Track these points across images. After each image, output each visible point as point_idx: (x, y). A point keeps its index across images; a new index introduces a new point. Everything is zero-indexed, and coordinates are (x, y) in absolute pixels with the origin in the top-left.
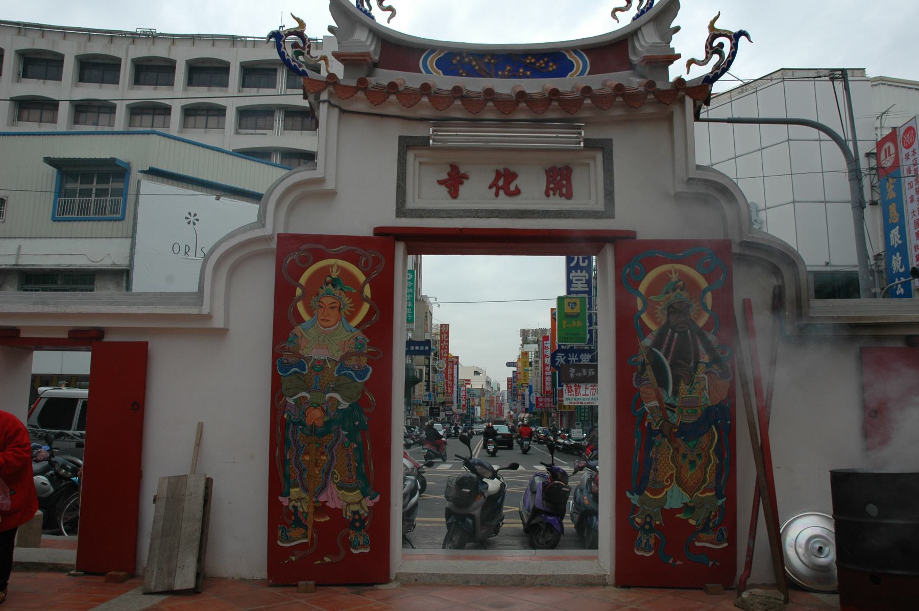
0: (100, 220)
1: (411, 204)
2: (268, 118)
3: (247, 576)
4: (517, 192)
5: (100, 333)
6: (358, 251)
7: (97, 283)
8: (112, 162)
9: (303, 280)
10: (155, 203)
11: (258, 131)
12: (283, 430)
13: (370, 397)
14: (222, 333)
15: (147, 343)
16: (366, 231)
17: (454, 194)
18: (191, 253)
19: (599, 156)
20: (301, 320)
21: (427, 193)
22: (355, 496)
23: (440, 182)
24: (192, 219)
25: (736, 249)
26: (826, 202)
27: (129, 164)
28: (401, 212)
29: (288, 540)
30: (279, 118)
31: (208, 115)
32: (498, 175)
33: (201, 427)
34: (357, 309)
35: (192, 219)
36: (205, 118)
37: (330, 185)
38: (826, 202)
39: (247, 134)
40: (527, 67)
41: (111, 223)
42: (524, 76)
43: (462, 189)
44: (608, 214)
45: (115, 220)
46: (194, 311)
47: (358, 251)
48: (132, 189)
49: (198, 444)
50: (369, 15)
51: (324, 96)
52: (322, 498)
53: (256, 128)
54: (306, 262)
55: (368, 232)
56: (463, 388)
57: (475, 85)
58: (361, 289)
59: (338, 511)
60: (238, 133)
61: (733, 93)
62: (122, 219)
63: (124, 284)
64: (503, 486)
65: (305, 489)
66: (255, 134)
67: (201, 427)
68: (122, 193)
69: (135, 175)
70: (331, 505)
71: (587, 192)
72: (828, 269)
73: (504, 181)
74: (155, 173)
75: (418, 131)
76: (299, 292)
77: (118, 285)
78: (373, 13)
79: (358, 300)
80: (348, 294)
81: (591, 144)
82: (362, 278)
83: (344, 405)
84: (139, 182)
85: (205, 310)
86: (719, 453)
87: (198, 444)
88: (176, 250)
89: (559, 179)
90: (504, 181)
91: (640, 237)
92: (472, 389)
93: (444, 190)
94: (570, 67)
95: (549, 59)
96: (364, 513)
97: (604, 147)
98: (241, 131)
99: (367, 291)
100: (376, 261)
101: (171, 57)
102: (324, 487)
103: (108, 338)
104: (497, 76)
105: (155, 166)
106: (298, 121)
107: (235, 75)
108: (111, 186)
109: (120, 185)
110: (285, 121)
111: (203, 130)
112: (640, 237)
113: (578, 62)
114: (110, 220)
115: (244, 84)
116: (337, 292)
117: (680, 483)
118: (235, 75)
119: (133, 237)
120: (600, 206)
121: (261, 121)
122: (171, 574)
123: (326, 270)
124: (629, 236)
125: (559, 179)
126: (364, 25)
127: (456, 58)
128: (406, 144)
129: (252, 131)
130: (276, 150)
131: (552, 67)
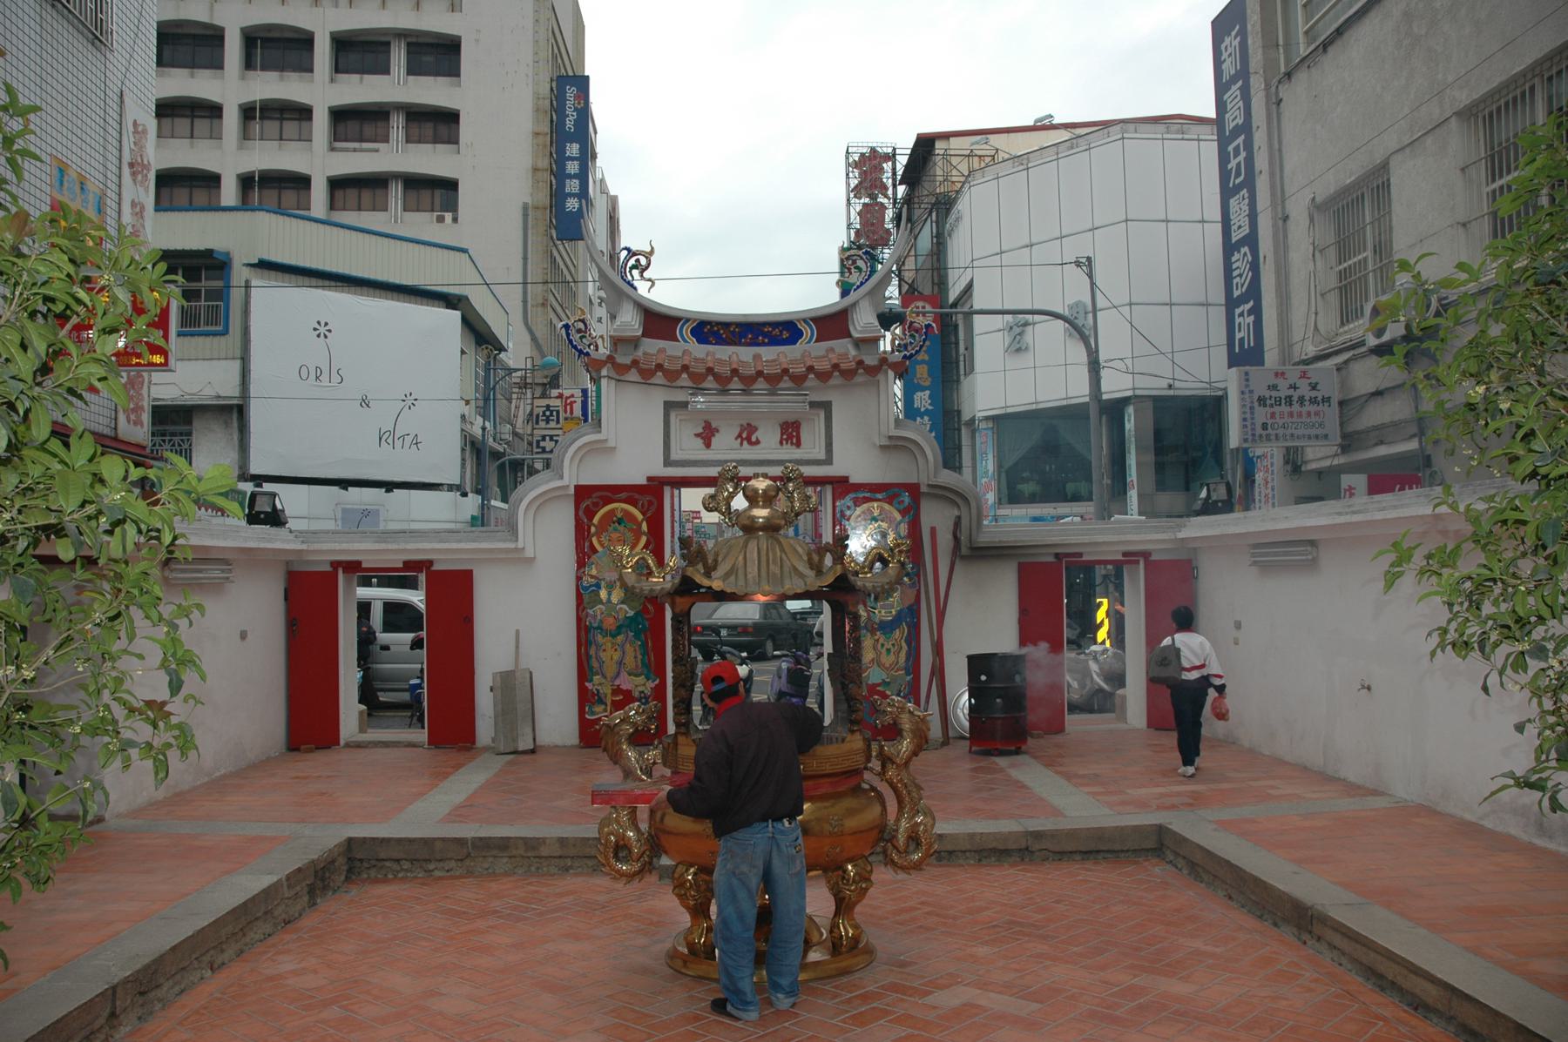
0: (192, 335)
1: (674, 456)
2: (380, 124)
3: (559, 743)
4: (758, 442)
5: (431, 562)
6: (637, 496)
7: (197, 424)
8: (209, 253)
9: (596, 521)
10: (275, 310)
11: (365, 145)
12: (585, 634)
13: (650, 607)
14: (532, 560)
15: (471, 572)
16: (640, 480)
17: (708, 445)
18: (325, 377)
19: (822, 415)
20: (595, 551)
21: (687, 445)
22: (641, 679)
23: (697, 435)
24: (322, 330)
25: (924, 489)
26: (1171, 305)
27: (228, 254)
28: (668, 462)
29: (593, 713)
30: (397, 123)
31: (282, 119)
32: (743, 429)
33: (517, 632)
34: (638, 540)
35: (322, 330)
36: (277, 123)
37: (611, 444)
38: (1171, 305)
39: (347, 150)
40: (765, 335)
41: (209, 339)
42: (763, 344)
43: (714, 440)
44: (828, 460)
45: (215, 334)
46: (512, 546)
47: (637, 496)
48: (236, 295)
49: (517, 647)
50: (632, 285)
51: (604, 372)
52: (617, 682)
53: (362, 140)
54: (598, 506)
55: (642, 481)
56: (689, 526)
57: (724, 353)
58: (640, 525)
59: (629, 692)
60: (332, 149)
61: (1062, 148)
62: (225, 333)
63: (235, 424)
64: (751, 672)
65: (604, 676)
66: (362, 150)
67: (517, 632)
68: (221, 295)
69: (239, 274)
70: (624, 687)
71: (812, 445)
72: (1171, 393)
73: (747, 435)
74: (265, 265)
75: (680, 396)
76: (593, 529)
77: (227, 424)
78: (636, 283)
79: (638, 533)
80: (631, 530)
81: (813, 405)
82: (640, 517)
83: (631, 613)
84: (247, 286)
85: (520, 545)
86: (909, 642)
87: (517, 647)
88: (304, 376)
89: (791, 432)
90: (747, 435)
91: (852, 481)
92: (704, 525)
93: (700, 442)
94: (800, 334)
95: (781, 330)
96: (648, 692)
97: (826, 407)
98: (338, 145)
99: (645, 527)
100: (650, 503)
101: (217, 22)
102: (618, 674)
103: (435, 568)
104: (740, 344)
105: (266, 257)
106: (428, 128)
107: (323, 52)
108: (204, 284)
109: (219, 284)
110: (407, 128)
111: (276, 143)
112: (852, 481)
113: (807, 331)
114: (207, 334)
115: (338, 68)
116: (620, 528)
117: (880, 664)
118: (323, 52)
119: (245, 360)
120: (822, 456)
121: (369, 129)
122: (515, 740)
123: (612, 512)
124: (845, 480)
125: (791, 432)
126: (629, 297)
127: (710, 330)
128: (669, 406)
129: (356, 145)
130: (396, 176)
131: (785, 335)
